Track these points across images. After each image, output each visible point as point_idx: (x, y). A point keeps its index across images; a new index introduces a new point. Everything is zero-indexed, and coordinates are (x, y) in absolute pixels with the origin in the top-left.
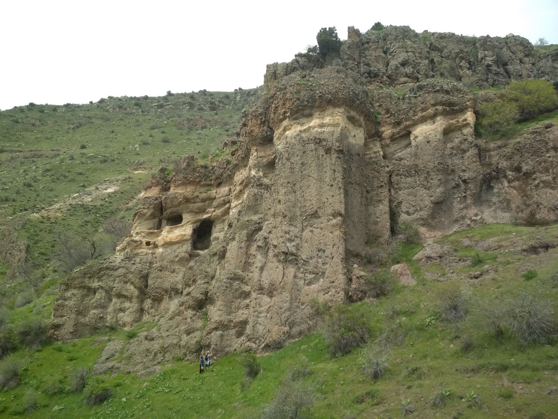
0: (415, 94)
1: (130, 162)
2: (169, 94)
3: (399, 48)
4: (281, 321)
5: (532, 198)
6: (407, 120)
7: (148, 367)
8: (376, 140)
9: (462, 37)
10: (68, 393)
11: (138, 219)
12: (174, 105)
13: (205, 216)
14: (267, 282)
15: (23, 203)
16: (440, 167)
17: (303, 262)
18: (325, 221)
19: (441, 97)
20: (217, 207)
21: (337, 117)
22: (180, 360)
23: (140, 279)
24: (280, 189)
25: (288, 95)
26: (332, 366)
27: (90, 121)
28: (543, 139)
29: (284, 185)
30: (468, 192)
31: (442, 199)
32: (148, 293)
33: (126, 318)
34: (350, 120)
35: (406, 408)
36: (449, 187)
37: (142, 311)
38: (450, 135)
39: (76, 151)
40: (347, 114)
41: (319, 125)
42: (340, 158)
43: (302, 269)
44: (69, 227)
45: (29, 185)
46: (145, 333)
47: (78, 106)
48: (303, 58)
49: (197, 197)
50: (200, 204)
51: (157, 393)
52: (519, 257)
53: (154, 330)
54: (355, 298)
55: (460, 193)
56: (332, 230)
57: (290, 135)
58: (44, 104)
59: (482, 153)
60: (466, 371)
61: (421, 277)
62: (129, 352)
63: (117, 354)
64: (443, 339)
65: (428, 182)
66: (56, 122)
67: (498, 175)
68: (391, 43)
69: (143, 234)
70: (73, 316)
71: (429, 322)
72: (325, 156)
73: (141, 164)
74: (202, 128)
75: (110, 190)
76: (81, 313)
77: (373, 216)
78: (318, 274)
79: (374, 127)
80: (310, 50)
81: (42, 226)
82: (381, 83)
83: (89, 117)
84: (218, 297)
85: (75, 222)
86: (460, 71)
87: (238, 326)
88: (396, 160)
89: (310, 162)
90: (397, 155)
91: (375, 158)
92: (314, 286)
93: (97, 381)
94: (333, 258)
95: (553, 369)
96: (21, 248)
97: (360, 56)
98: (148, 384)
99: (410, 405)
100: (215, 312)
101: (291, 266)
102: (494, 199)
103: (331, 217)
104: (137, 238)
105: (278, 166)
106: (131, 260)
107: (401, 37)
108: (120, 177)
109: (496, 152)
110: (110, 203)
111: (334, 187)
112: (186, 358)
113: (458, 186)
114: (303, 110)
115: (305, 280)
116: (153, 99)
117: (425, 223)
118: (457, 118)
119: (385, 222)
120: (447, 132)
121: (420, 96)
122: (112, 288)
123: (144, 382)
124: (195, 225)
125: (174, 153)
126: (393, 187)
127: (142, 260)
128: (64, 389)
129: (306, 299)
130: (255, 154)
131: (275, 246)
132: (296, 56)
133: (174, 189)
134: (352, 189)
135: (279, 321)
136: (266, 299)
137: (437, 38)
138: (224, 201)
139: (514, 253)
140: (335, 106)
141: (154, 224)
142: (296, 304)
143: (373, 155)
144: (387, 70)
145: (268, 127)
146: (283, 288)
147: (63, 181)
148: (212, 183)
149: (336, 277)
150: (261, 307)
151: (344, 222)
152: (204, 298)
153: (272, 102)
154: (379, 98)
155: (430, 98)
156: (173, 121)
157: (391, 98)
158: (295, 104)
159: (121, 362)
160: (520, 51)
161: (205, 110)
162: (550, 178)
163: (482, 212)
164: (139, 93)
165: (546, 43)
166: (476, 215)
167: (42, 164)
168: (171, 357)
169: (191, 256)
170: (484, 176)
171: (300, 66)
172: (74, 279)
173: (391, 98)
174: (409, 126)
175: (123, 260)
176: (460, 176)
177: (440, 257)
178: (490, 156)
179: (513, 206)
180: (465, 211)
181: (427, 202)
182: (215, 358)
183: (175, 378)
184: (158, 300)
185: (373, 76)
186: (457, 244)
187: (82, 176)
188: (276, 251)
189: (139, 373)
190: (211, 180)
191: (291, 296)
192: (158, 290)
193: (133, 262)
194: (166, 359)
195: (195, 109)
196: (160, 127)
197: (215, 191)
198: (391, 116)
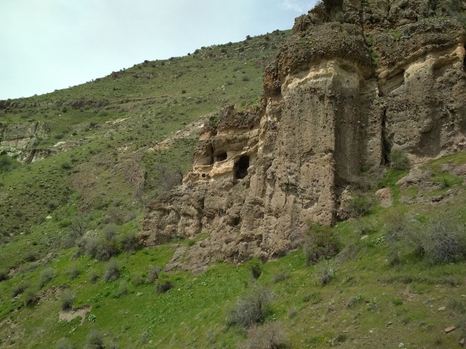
0: (409, 35)
1: (218, 101)
2: (249, 38)
4: (284, 236)
6: (400, 60)
7: (199, 267)
8: (373, 80)
10: (147, 284)
11: (196, 157)
12: (252, 47)
13: (243, 153)
15: (143, 141)
17: (301, 190)
18: (319, 156)
20: (250, 145)
21: (330, 68)
22: (221, 262)
23: (198, 202)
25: (289, 55)
26: (302, 272)
27: (189, 69)
30: (456, 121)
32: (204, 213)
33: (190, 230)
34: (343, 68)
35: (330, 307)
37: (201, 225)
38: (441, 69)
39: (178, 95)
40: (339, 64)
41: (314, 77)
43: (300, 196)
44: (174, 157)
46: (201, 242)
47: (180, 59)
49: (236, 138)
50: (239, 144)
53: (206, 240)
54: (342, 218)
55: (448, 122)
57: (291, 88)
58: (155, 60)
61: (397, 200)
62: (189, 256)
63: (181, 257)
65: (417, 115)
66: (164, 74)
69: (200, 169)
70: (155, 229)
71: (380, 240)
72: (319, 103)
73: (226, 102)
76: (161, 227)
78: (313, 200)
81: (155, 157)
82: (382, 27)
83: (188, 67)
85: (178, 153)
88: (390, 97)
89: (306, 109)
91: (371, 96)
92: (310, 208)
94: (324, 186)
95: (444, 283)
98: (196, 279)
99: (333, 306)
100: (244, 230)
103: (324, 153)
104: (196, 172)
105: (283, 114)
106: (192, 188)
111: (326, 128)
113: (446, 116)
114: (301, 65)
115: (303, 204)
116: (236, 44)
117: (414, 151)
120: (437, 69)
121: (412, 37)
123: (195, 277)
127: (200, 188)
129: (304, 219)
130: (270, 103)
131: (280, 179)
132: (309, 12)
138: (255, 140)
140: (328, 58)
141: (208, 161)
142: (296, 223)
143: (370, 94)
146: (285, 211)
150: (271, 225)
151: (334, 157)
153: (278, 61)
154: (377, 43)
155: (421, 39)
156: (251, 61)
157: (387, 41)
158: (294, 61)
159: (183, 262)
167: (155, 108)
168: (215, 260)
169: (235, 183)
171: (311, 21)
173: (387, 41)
174: (402, 65)
175: (186, 189)
176: (447, 106)
177: (419, 181)
180: (452, 138)
181: (416, 132)
183: (214, 275)
184: (211, 217)
185: (374, 21)
187: (183, 116)
188: (281, 182)
189: (193, 271)
190: (246, 124)
191: (292, 217)
192: (211, 210)
193: (194, 190)
194: (212, 261)
195: (270, 48)
196: (241, 69)
197: (248, 133)
198: (386, 58)
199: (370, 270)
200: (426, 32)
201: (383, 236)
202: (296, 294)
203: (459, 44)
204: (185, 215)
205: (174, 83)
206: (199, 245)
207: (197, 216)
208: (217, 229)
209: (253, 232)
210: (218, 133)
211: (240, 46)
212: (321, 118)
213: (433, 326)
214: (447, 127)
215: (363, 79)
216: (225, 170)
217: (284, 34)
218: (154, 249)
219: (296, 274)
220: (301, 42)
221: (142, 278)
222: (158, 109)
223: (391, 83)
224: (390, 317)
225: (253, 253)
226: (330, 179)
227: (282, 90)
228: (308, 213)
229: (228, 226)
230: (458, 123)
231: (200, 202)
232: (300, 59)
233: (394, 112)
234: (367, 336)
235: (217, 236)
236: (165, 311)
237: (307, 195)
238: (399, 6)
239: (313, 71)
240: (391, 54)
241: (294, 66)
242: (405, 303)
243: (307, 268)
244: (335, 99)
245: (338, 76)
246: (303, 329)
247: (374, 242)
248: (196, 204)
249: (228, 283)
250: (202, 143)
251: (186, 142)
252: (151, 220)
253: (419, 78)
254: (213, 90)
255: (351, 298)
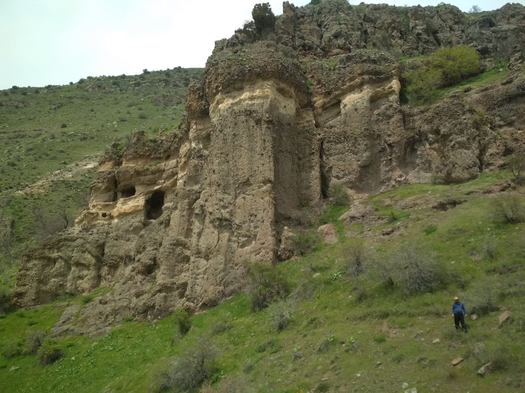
0: (345, 64)
1: (109, 139)
2: (146, 71)
3: (332, 20)
4: (216, 281)
5: (449, 158)
6: (336, 89)
7: (99, 329)
8: (309, 110)
9: (394, 7)
10: (26, 354)
12: (150, 82)
13: (156, 188)
14: (204, 246)
15: (8, 182)
16: (366, 133)
17: (236, 226)
19: (367, 66)
20: (166, 178)
21: (266, 90)
22: (130, 320)
23: (96, 248)
24: (215, 159)
25: (220, 71)
26: (248, 320)
27: (71, 101)
28: (460, 102)
29: (218, 155)
31: (368, 163)
32: (104, 261)
33: (85, 284)
34: (280, 92)
35: (296, 354)
36: (376, 151)
37: (99, 277)
38: (377, 102)
39: (57, 130)
40: (276, 86)
41: (249, 98)
42: (269, 128)
43: (235, 233)
44: (51, 202)
45: (13, 165)
46: (100, 298)
47: (59, 88)
48: (243, 34)
49: (148, 169)
50: (151, 177)
51: (103, 351)
52: (429, 213)
53: (108, 294)
54: (283, 257)
55: (386, 156)
56: (263, 196)
57: (222, 108)
58: (27, 87)
59: (405, 118)
60: (355, 319)
61: (343, 235)
62: (84, 315)
64: (345, 291)
65: (356, 147)
67: (420, 138)
68: (325, 16)
69: (99, 207)
70: (35, 284)
71: (337, 276)
72: (255, 127)
74: (178, 103)
75: (89, 166)
76: (43, 281)
77: (305, 181)
78: (250, 238)
79: (306, 98)
80: (246, 26)
81: (26, 202)
82: (315, 55)
83: (69, 98)
84: (161, 262)
85: (57, 198)
86: (392, 40)
87: (181, 287)
88: (327, 128)
90: (328, 124)
91: (307, 126)
92: (246, 248)
93: (50, 343)
94: (263, 221)
95: (426, 314)
96: (6, 223)
97: (295, 30)
98: (97, 343)
99: (300, 352)
100: (161, 277)
101: (225, 230)
102: (418, 161)
103: (262, 184)
104: (94, 211)
105: (213, 138)
106: (89, 231)
107: (334, 10)
108: (99, 153)
109: (419, 116)
110: (90, 178)
112: (135, 319)
113: (384, 149)
114: (234, 84)
115: (239, 243)
116: (130, 77)
117: (353, 186)
118: (384, 86)
119: (316, 185)
120: (374, 100)
121: (348, 66)
122: (70, 258)
124: (147, 196)
125: (150, 129)
126: (325, 154)
127: (98, 230)
128: (22, 351)
131: (211, 213)
132: (236, 32)
133: (126, 164)
134: (283, 157)
135: (214, 282)
136: (203, 261)
137: (371, 9)
138: (172, 172)
139: (426, 210)
140: (265, 79)
142: (231, 265)
143: (306, 124)
144: (321, 42)
145: (206, 101)
146: (218, 251)
147: (45, 160)
148: (162, 156)
149: (266, 239)
150: (199, 269)
151: (273, 188)
152: (152, 263)
153: (206, 78)
154: (311, 70)
155: (357, 68)
157: (322, 69)
158: (226, 78)
159: (76, 325)
160: (450, 19)
161: (180, 87)
162: (465, 139)
163: (407, 174)
164: (117, 73)
165: (480, 10)
166: (401, 176)
167: (23, 143)
168: (121, 319)
169: (145, 225)
170: (408, 139)
171: (239, 41)
172: (35, 250)
173: (322, 69)
174: (339, 95)
175: (80, 231)
176: (385, 140)
177: (363, 216)
178: (414, 121)
179: (434, 166)
181: (355, 166)
182: (159, 317)
183: (121, 337)
184: (114, 267)
185: (307, 49)
186: (378, 204)
187: (63, 154)
188: (212, 217)
189: (91, 334)
190: (160, 153)
191: (226, 258)
192: (114, 258)
193: (90, 233)
195: (171, 86)
196: (137, 105)
197: (164, 164)
198: (322, 86)
199: (334, 308)
200: (362, 62)
201: (339, 271)
202: (244, 345)
203: (395, 77)
204: (78, 264)
205: (51, 115)
206: (98, 301)
207: (95, 265)
208: (122, 281)
209: (174, 280)
210: (124, 163)
211: (135, 80)
212: (258, 144)
213: (436, 361)
214: (385, 162)
215: (299, 106)
216: (133, 208)
217: (187, 71)
218: (32, 311)
219: (240, 322)
220: (234, 57)
221: (18, 348)
222: (28, 144)
223: (327, 114)
224: (376, 356)
225: (174, 306)
226: (270, 212)
227: (210, 112)
228: (245, 253)
229: (140, 276)
230: (396, 158)
231: (99, 248)
232: (233, 76)
233: (331, 145)
234: (355, 380)
235: (122, 289)
236: (54, 387)
237: (243, 232)
238: (332, 35)
239: (247, 91)
240: (327, 83)
241: (226, 83)
242: (388, 340)
243: (252, 315)
244: (272, 124)
245: (275, 99)
246: (267, 383)
247: (331, 279)
248: (94, 250)
249: (143, 344)
250: (103, 175)
251: (67, 184)
252: (28, 273)
253: (356, 110)
254: (103, 126)
255: (323, 339)
